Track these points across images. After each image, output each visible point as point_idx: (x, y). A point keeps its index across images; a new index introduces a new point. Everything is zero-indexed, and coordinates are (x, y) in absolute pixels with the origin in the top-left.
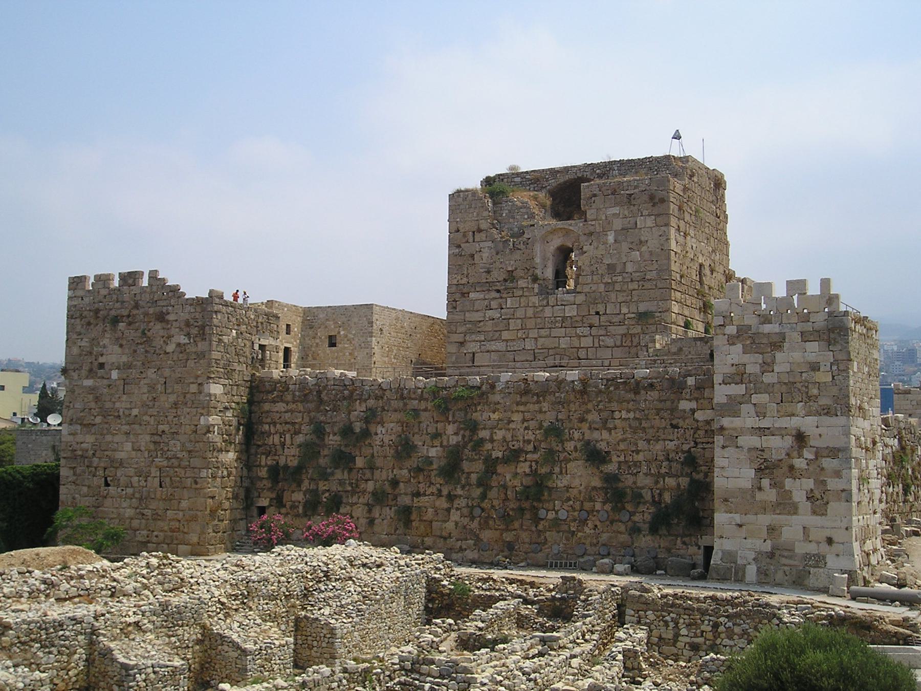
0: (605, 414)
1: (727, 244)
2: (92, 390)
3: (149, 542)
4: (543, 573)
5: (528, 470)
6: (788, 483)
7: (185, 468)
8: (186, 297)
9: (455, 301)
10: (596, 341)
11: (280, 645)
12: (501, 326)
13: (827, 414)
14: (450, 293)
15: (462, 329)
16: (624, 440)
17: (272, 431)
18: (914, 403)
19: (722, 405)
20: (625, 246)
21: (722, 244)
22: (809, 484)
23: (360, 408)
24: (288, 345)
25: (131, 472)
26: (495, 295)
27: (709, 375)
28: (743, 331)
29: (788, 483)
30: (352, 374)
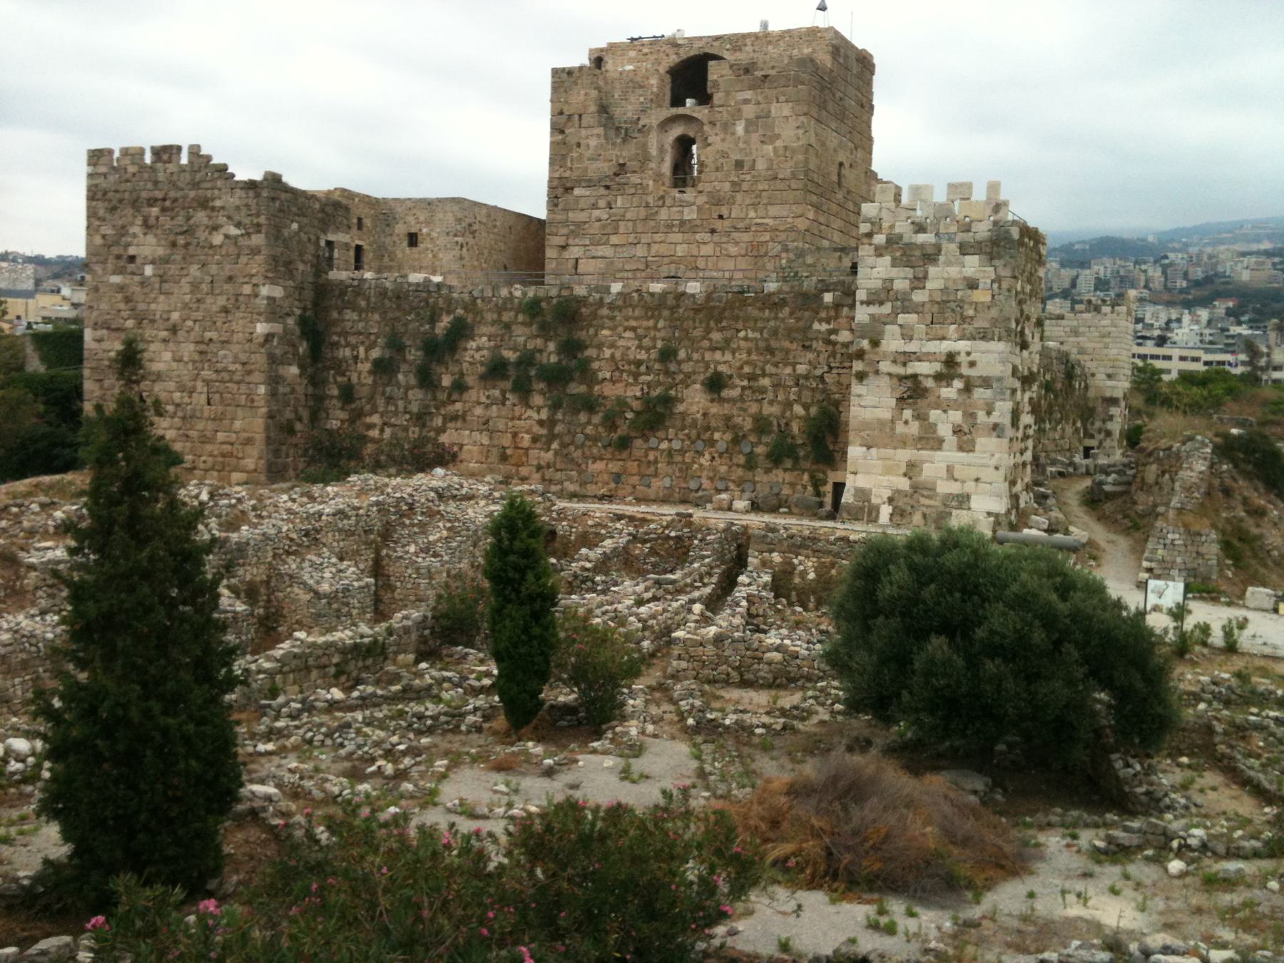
0: (728, 334)
1: (870, 139)
2: (121, 288)
3: (194, 468)
4: (654, 508)
5: (638, 394)
6: (934, 415)
7: (238, 383)
8: (237, 178)
9: (556, 197)
10: (718, 249)
11: (360, 587)
12: (609, 230)
13: (983, 338)
14: (551, 188)
15: (565, 231)
16: (747, 363)
17: (343, 342)
18: (1068, 329)
19: (862, 326)
20: (755, 137)
21: (864, 142)
22: (956, 416)
23: (445, 322)
24: (360, 243)
25: (171, 385)
26: (603, 191)
27: (850, 293)
28: (893, 241)
29: (934, 415)
30: (437, 279)
